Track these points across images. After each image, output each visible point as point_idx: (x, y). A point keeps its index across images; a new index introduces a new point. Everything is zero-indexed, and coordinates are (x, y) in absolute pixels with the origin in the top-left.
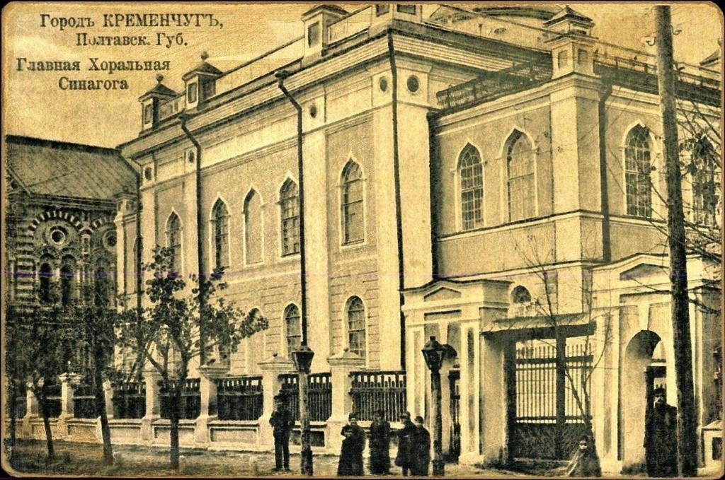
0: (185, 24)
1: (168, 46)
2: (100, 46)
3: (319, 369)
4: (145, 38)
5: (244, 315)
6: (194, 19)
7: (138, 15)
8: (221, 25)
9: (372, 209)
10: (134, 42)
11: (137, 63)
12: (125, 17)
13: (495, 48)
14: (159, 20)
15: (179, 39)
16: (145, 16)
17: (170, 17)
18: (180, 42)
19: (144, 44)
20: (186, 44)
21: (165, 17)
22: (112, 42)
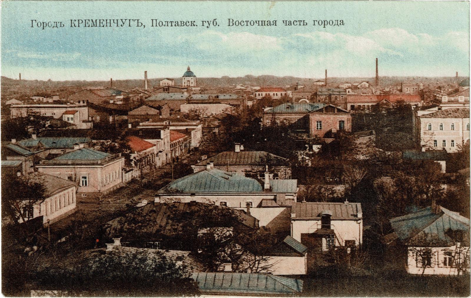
0: (121, 25)
1: (207, 27)
2: (166, 27)
3: (309, 223)
4: (194, 22)
5: (370, 138)
6: (127, 22)
7: (92, 20)
8: (144, 26)
9: (431, 115)
10: (188, 24)
11: (259, 25)
12: (84, 21)
13: (162, 125)
14: (105, 23)
15: (215, 22)
16: (96, 20)
17: (112, 21)
18: (215, 24)
19: (194, 25)
20: (219, 25)
21: (108, 21)
22: (173, 24)
